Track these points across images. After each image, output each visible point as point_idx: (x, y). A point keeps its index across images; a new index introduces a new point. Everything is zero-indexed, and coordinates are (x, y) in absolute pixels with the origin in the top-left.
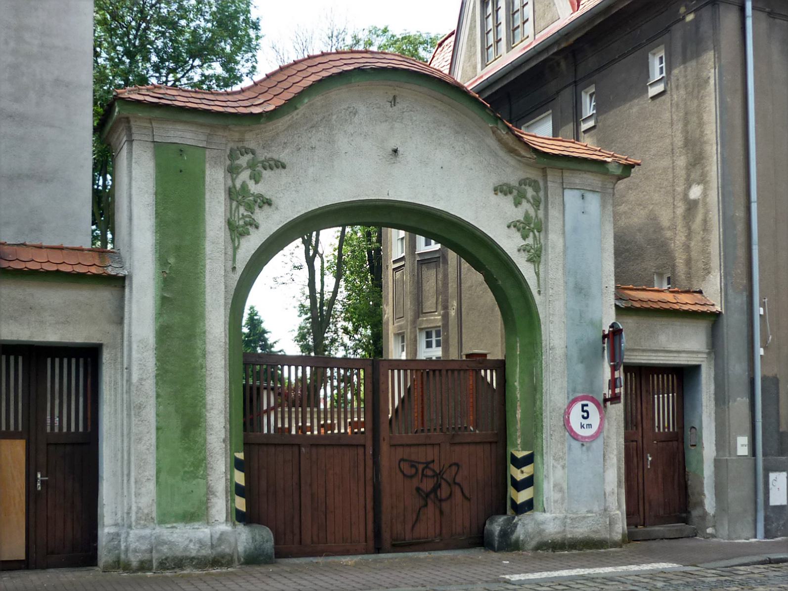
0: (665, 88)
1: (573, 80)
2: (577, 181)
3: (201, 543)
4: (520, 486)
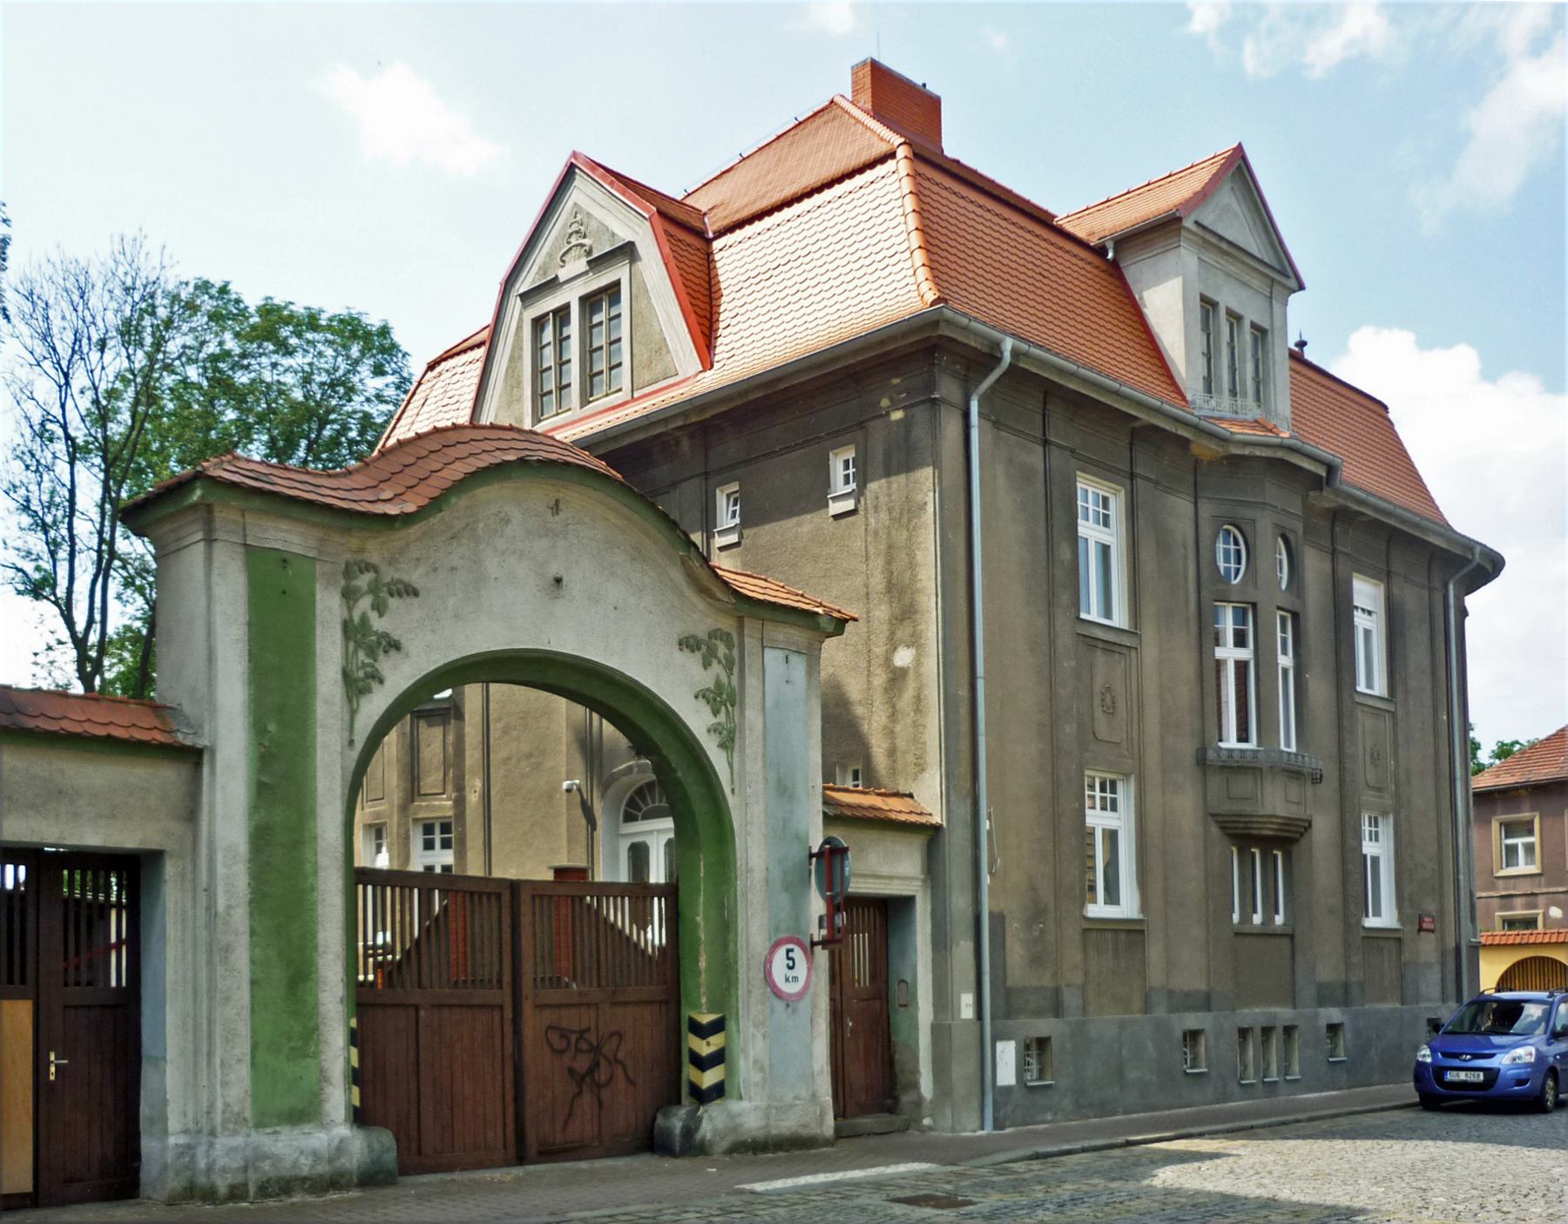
0: (856, 505)
1: (703, 470)
2: (781, 637)
3: (315, 1155)
4: (702, 1063)
